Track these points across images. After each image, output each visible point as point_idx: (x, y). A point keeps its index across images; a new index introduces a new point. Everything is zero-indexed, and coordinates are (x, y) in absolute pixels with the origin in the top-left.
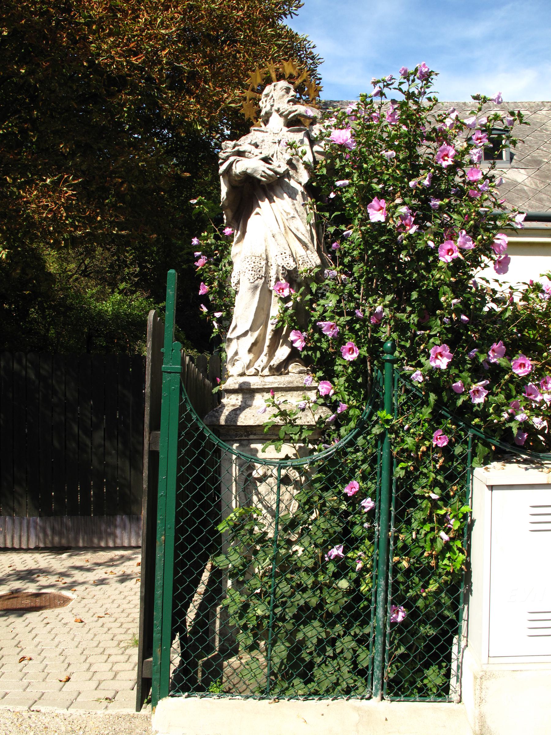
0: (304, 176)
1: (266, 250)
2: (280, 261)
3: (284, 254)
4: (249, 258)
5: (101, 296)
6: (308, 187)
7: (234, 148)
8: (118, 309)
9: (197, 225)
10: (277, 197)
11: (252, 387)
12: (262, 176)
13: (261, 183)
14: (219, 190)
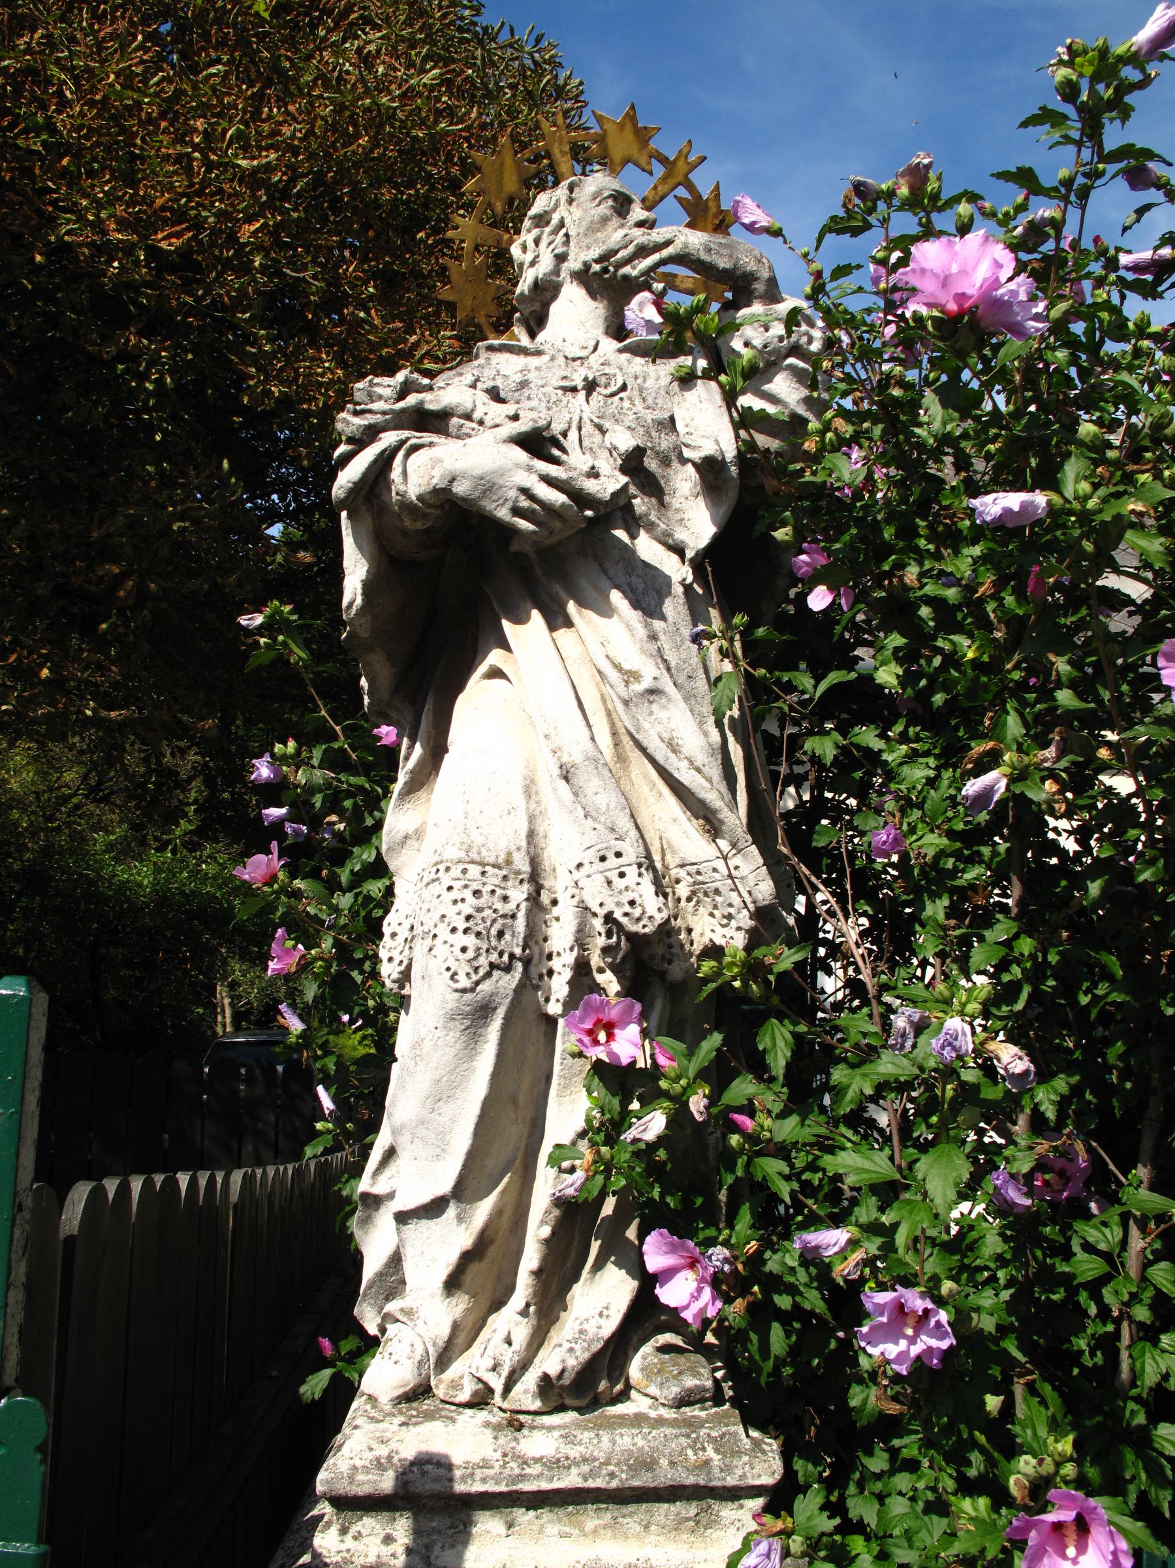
0: (698, 525)
1: (531, 834)
2: (590, 889)
3: (612, 861)
4: (456, 871)
5: (128, 850)
7: (401, 396)
8: (167, 880)
9: (277, 702)
10: (582, 603)
11: (460, 1488)
12: (517, 511)
14: (337, 574)
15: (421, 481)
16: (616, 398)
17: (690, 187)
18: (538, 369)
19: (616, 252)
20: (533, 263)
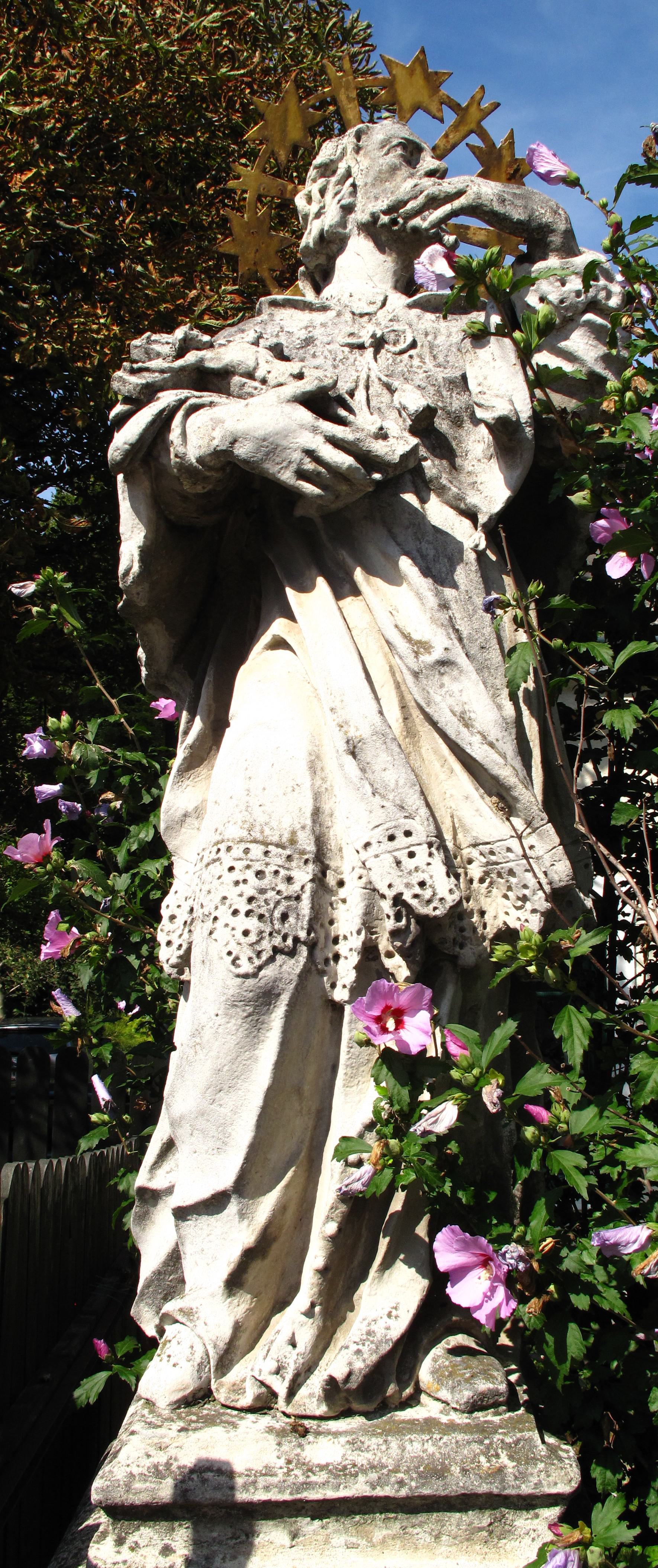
1: (316, 812)
2: (379, 871)
3: (402, 841)
4: (237, 851)
6: (505, 528)
7: (181, 353)
10: (370, 571)
11: (242, 1496)
12: (301, 474)
13: (299, 512)
14: (113, 540)
15: (200, 442)
16: (406, 356)
17: (483, 134)
18: (323, 325)
19: (405, 203)
20: (318, 215)
